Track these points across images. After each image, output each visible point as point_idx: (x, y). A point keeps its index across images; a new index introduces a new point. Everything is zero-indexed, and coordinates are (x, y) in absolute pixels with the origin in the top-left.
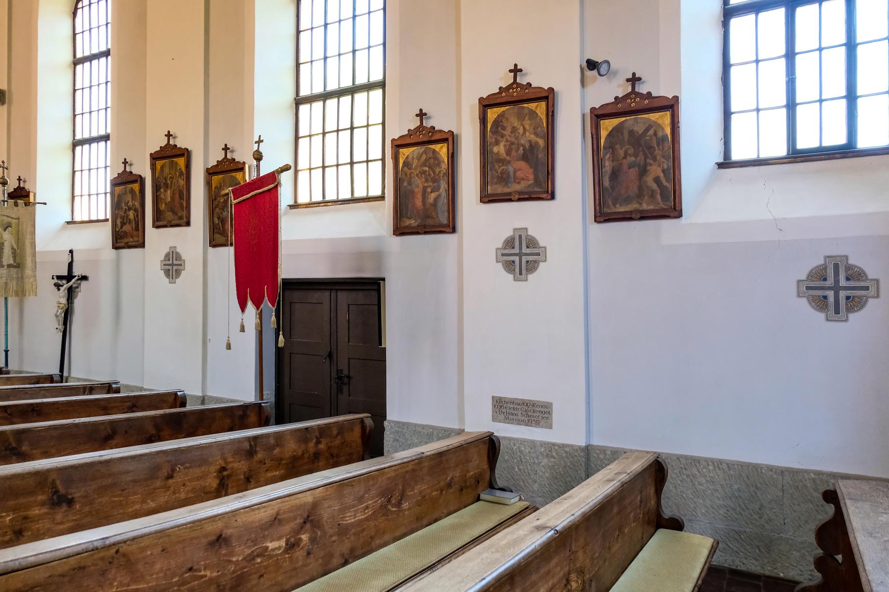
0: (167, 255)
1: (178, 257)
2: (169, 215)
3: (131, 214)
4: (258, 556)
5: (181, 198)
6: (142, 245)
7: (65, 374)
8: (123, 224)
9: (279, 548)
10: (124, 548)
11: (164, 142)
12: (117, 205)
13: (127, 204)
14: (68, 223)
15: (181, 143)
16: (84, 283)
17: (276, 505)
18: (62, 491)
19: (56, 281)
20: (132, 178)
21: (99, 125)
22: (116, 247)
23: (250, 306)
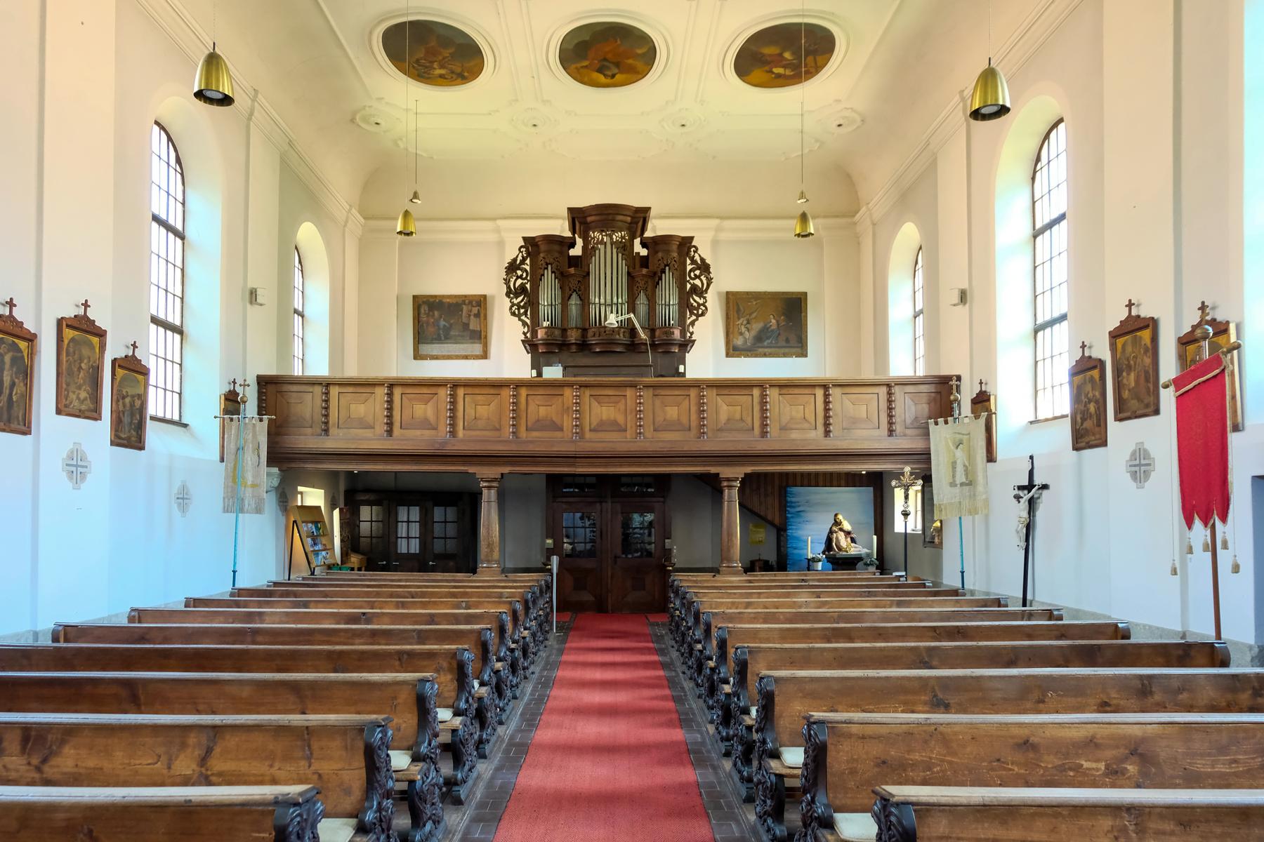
0: (1133, 454)
1: (1146, 454)
2: (1134, 404)
3: (1092, 407)
4: (1071, 769)
5: (1147, 380)
6: (1104, 444)
7: (1029, 597)
8: (1083, 420)
9: (1098, 770)
10: (941, 728)
11: (1124, 315)
12: (1078, 396)
13: (1086, 395)
14: (1031, 423)
15: (1145, 312)
16: (1045, 492)
17: (1091, 729)
18: (940, 696)
19: (1016, 492)
20: (1091, 365)
21: (1058, 303)
22: (1076, 448)
23: (1198, 523)
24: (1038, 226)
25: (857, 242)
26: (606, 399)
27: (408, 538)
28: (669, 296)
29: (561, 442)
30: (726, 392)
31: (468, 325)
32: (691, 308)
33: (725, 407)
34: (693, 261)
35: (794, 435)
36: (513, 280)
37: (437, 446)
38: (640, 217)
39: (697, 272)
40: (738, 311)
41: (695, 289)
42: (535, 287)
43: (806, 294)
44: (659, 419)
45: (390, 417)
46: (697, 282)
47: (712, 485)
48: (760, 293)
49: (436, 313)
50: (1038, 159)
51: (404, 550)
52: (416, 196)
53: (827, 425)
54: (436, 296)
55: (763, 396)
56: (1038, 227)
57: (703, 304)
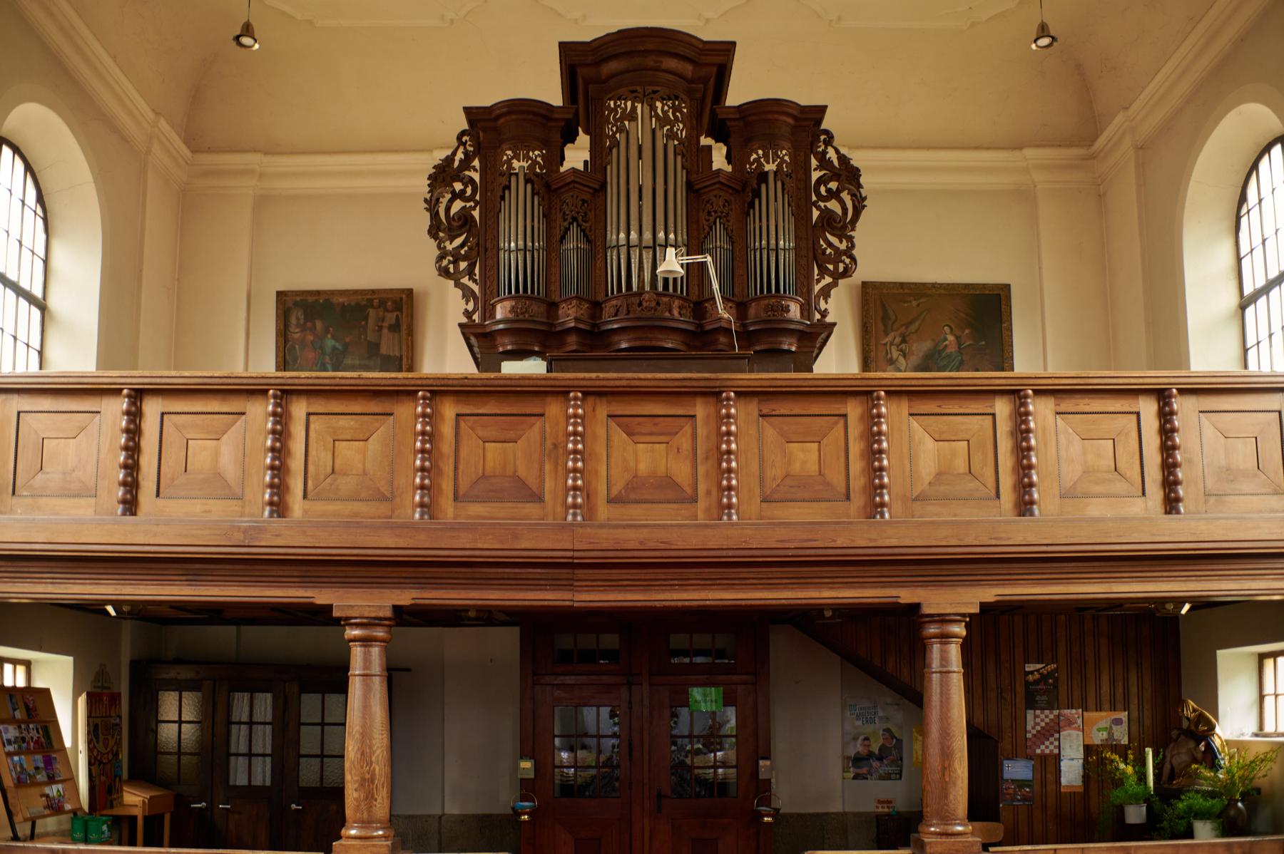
24: (1248, 290)
25: (1100, 196)
26: (648, 425)
27: (250, 755)
28: (776, 235)
29: (537, 529)
30: (931, 406)
31: (377, 346)
32: (819, 258)
33: (929, 444)
34: (824, 163)
35: (1096, 509)
36: (444, 201)
37: (238, 538)
38: (717, 60)
39: (833, 185)
40: (885, 318)
41: (829, 221)
42: (491, 214)
43: (1007, 287)
44: (775, 472)
45: (132, 467)
46: (833, 205)
47: (903, 630)
48: (924, 285)
49: (319, 324)
50: (1243, 198)
51: (241, 780)
52: (247, 30)
53: (1170, 483)
54: (318, 293)
55: (1020, 417)
56: (1248, 290)
57: (849, 252)
